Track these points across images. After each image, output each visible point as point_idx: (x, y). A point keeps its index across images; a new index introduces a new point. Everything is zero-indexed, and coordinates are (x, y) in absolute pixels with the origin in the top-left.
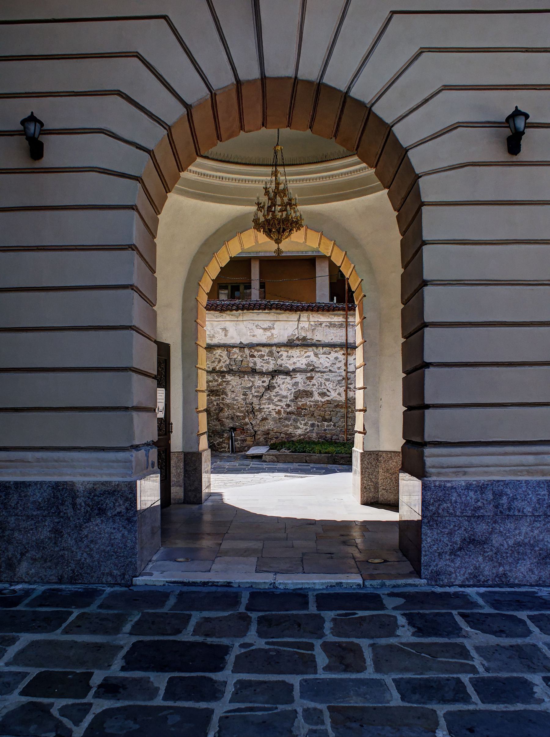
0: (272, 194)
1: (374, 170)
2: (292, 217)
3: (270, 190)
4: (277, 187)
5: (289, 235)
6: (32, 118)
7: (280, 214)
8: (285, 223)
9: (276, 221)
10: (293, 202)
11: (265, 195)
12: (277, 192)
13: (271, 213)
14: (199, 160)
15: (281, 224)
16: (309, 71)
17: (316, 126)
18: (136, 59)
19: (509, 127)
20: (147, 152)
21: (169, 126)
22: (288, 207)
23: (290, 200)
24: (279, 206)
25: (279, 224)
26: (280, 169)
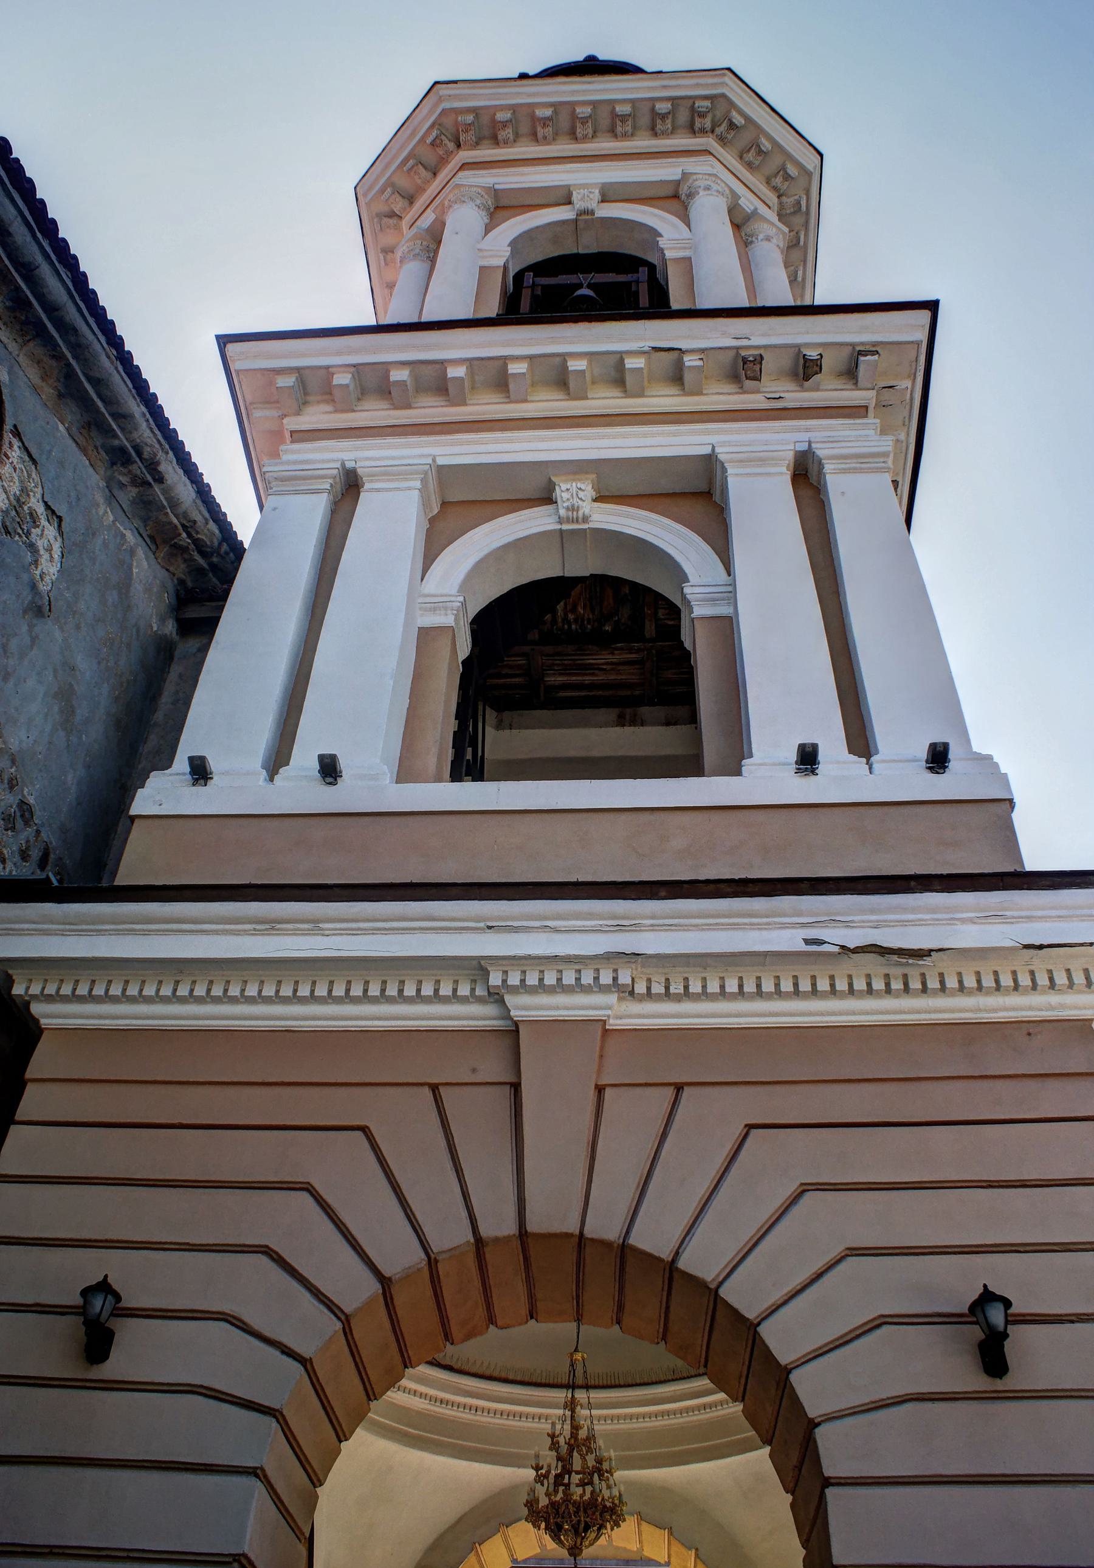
0: (564, 1449)
1: (739, 1407)
2: (603, 1499)
3: (562, 1440)
4: (574, 1435)
5: (597, 1538)
6: (104, 1287)
7: (580, 1490)
8: (590, 1512)
9: (570, 1506)
10: (605, 1466)
11: (551, 1449)
12: (575, 1443)
13: (561, 1488)
14: (423, 1369)
15: (581, 1513)
16: (605, 1225)
17: (626, 1319)
18: (305, 1194)
19: (976, 1323)
20: (299, 1362)
21: (345, 1314)
22: (596, 1475)
23: (599, 1461)
24: (577, 1473)
25: (576, 1513)
26: (581, 1395)
